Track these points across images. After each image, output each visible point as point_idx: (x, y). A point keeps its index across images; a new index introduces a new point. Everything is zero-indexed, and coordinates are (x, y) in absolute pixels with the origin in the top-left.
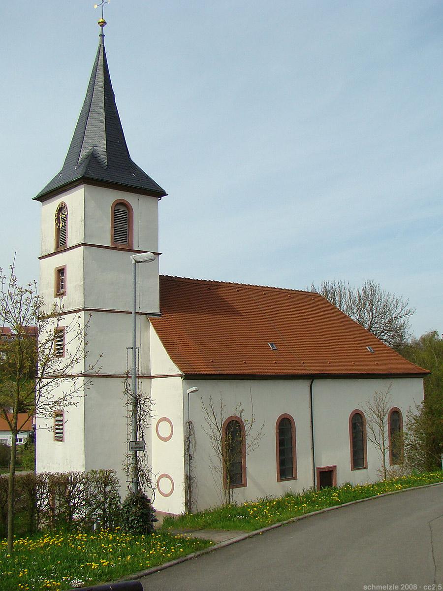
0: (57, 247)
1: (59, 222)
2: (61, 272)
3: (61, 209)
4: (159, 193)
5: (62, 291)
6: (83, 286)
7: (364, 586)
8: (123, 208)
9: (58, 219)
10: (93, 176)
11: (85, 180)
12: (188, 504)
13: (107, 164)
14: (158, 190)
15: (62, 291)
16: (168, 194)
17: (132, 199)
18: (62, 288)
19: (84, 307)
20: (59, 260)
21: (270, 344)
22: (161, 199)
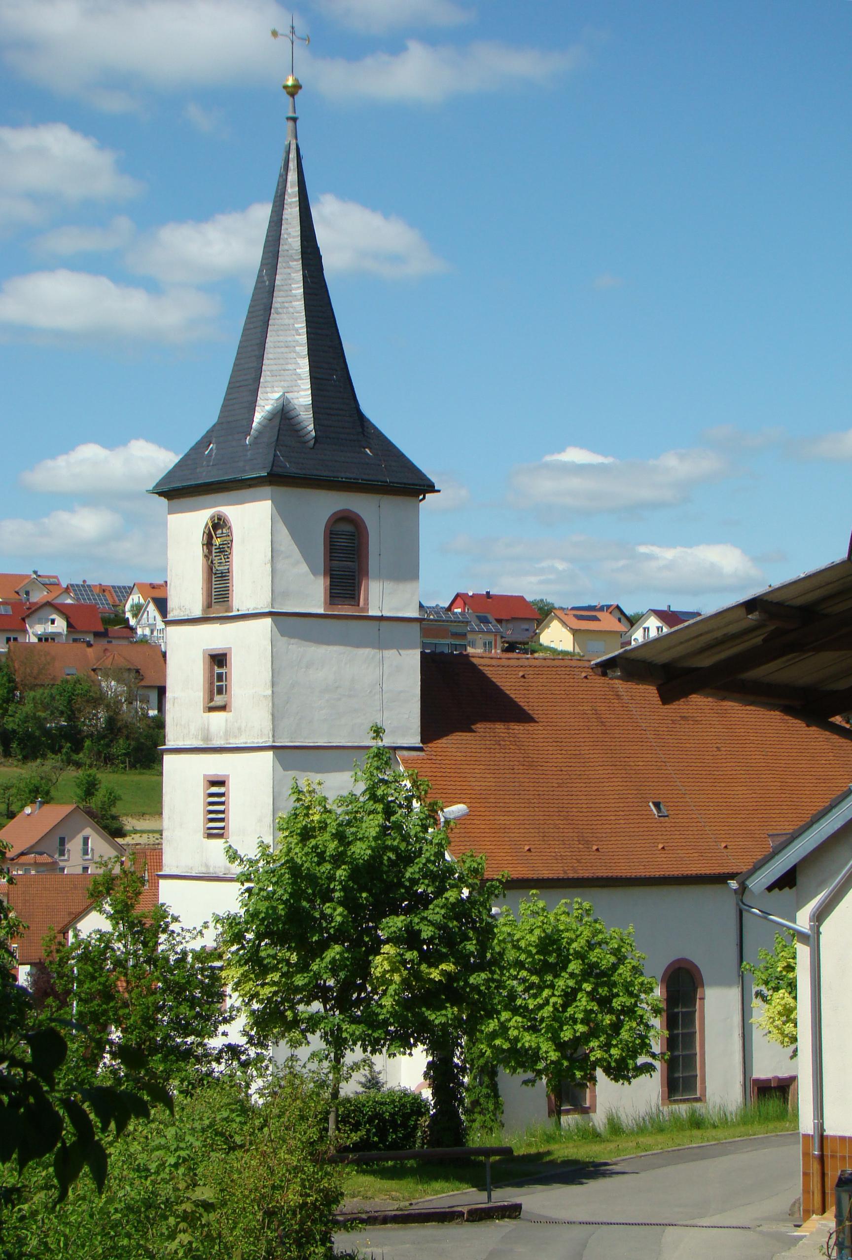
0: (208, 606)
1: (210, 552)
2: (219, 660)
3: (219, 524)
4: (417, 486)
5: (219, 700)
6: (270, 698)
7: (415, 953)
8: (349, 528)
9: (208, 543)
10: (290, 467)
11: (277, 478)
12: (559, 1119)
13: (313, 433)
14: (421, 482)
15: (219, 700)
16: (439, 491)
17: (363, 506)
18: (220, 691)
19: (274, 741)
20: (215, 636)
21: (653, 803)
22: (424, 498)
